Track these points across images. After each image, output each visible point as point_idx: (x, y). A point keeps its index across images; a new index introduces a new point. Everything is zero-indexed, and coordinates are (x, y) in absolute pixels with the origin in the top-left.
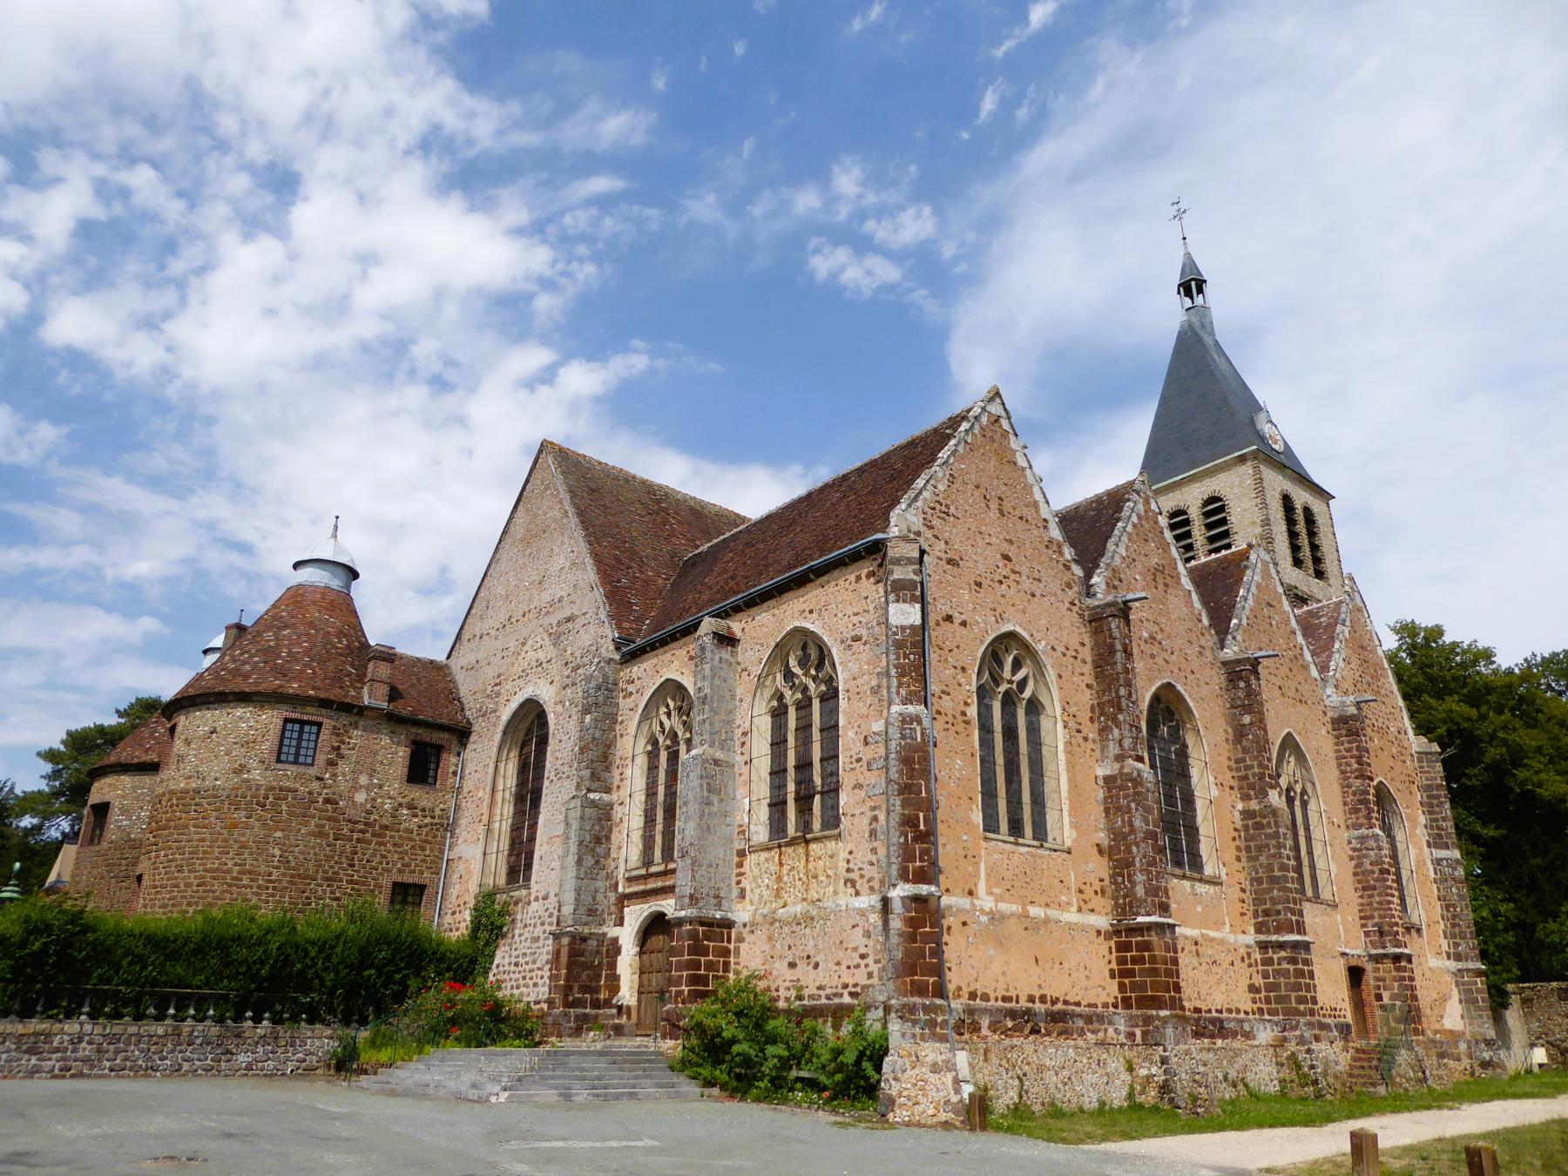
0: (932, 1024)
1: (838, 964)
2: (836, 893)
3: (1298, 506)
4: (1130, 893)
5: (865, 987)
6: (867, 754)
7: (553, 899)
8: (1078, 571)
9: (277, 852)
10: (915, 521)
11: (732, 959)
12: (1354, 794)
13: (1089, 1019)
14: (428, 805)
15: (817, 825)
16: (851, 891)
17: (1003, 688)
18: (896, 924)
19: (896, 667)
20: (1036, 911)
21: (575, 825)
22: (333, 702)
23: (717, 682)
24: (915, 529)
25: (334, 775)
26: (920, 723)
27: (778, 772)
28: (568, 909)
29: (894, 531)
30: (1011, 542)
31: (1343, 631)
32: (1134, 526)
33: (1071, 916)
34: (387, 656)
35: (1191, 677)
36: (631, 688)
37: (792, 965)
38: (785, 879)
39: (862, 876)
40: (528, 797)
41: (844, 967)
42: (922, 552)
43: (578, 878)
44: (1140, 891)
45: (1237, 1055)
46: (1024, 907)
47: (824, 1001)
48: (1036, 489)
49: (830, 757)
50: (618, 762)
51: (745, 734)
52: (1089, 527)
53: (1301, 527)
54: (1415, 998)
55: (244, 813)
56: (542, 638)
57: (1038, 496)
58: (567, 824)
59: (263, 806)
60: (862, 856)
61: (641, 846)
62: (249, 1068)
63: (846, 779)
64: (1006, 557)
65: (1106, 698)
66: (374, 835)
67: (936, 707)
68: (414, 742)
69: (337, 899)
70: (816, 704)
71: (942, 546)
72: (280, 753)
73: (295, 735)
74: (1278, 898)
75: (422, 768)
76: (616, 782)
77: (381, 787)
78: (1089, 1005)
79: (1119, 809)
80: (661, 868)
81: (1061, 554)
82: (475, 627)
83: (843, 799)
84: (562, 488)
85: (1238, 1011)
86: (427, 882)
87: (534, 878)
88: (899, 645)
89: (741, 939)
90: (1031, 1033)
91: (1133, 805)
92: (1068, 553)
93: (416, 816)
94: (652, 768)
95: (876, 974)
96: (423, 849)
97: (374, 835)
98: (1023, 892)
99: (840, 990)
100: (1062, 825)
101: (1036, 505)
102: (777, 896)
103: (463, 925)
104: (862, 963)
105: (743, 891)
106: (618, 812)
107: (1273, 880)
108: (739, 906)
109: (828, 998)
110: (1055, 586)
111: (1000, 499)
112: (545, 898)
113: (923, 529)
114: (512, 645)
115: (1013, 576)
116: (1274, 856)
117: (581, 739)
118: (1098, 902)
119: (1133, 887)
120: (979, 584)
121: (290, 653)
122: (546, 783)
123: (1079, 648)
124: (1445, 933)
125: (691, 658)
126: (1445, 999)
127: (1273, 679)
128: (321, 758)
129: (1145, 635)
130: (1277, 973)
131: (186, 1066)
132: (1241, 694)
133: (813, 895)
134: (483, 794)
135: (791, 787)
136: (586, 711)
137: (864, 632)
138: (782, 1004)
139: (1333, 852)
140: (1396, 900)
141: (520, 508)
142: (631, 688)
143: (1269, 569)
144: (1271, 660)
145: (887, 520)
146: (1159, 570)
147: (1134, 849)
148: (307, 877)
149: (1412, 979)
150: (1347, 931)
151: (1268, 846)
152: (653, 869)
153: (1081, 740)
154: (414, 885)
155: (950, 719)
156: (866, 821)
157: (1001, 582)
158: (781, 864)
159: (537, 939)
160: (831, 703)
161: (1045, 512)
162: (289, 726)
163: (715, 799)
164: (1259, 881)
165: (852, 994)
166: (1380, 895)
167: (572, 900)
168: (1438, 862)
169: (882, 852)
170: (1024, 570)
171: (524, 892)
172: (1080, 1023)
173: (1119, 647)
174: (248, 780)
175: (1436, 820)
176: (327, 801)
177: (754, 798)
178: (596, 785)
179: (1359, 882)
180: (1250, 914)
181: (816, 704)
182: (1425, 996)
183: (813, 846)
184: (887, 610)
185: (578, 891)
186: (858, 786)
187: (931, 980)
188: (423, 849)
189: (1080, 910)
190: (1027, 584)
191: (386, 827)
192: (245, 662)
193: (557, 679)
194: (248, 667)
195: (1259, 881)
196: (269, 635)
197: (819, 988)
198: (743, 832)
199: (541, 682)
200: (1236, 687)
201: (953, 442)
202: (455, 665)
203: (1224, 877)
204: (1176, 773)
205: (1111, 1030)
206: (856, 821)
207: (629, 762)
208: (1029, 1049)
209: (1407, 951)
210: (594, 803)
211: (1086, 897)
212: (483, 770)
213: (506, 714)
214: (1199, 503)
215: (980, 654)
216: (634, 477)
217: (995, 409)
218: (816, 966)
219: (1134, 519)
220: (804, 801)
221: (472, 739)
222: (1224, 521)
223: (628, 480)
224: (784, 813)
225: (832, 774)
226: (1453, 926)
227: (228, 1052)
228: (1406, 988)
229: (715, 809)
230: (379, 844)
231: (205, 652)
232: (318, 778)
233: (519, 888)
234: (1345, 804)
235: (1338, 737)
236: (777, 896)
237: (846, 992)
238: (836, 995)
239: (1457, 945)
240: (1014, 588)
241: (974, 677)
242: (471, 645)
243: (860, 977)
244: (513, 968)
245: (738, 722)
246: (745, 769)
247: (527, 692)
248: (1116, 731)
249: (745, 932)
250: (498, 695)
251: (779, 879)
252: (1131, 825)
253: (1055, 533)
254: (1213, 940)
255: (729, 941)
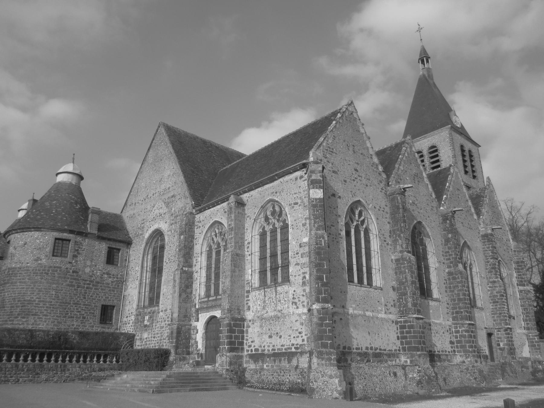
0: (330, 359)
1: (290, 336)
2: (288, 307)
3: (467, 149)
4: (406, 305)
5: (301, 345)
6: (302, 251)
7: (169, 311)
8: (384, 176)
9: (54, 293)
10: (320, 154)
11: (245, 335)
12: (490, 265)
13: (389, 356)
14: (115, 273)
15: (280, 280)
16: (295, 306)
17: (355, 223)
18: (315, 320)
19: (313, 215)
20: (368, 314)
21: (178, 281)
22: (75, 231)
23: (237, 222)
24: (319, 158)
25: (76, 261)
26: (323, 238)
27: (263, 258)
28: (176, 315)
29: (311, 159)
30: (358, 164)
31: (487, 200)
32: (406, 157)
33: (382, 315)
34: (98, 212)
35: (428, 219)
36: (200, 225)
37: (270, 337)
38: (267, 302)
39: (299, 301)
40: (157, 270)
41: (292, 337)
42: (323, 168)
43: (179, 302)
44: (410, 305)
45: (445, 368)
46: (364, 313)
47: (284, 351)
48: (367, 142)
49: (285, 251)
50: (195, 255)
51: (249, 243)
52: (388, 158)
53: (467, 158)
54: (513, 345)
55: (39, 277)
56: (161, 204)
57: (369, 145)
58: (175, 281)
59: (48, 274)
60: (300, 291)
61: (205, 289)
62: (47, 380)
63: (292, 261)
64: (356, 170)
65: (396, 228)
66: (93, 285)
67: (329, 231)
68: (109, 248)
69: (79, 312)
70: (279, 230)
71: (330, 165)
72: (54, 252)
73: (60, 245)
74: (464, 306)
75: (111, 258)
76: (194, 263)
77: (96, 266)
78: (389, 350)
79: (401, 272)
80: (214, 298)
81: (378, 169)
82: (132, 200)
83: (291, 269)
84: (168, 142)
85: (446, 351)
86: (116, 304)
87: (161, 302)
88: (314, 206)
89: (248, 327)
90: (367, 362)
91: (407, 271)
92: (380, 168)
93: (110, 277)
94: (209, 257)
95: (306, 340)
96: (114, 291)
97: (93, 285)
98: (364, 306)
99: (290, 346)
100: (377, 280)
101: (368, 148)
102: (264, 308)
103: (131, 322)
104: (300, 335)
105: (249, 307)
106: (195, 275)
107: (460, 300)
108: (248, 313)
109: (285, 349)
110: (376, 182)
111: (353, 146)
112: (166, 310)
113: (323, 158)
114: (149, 207)
115: (359, 178)
116: (460, 290)
117: (179, 246)
118: (393, 309)
119: (407, 303)
120: (345, 181)
121: (56, 211)
122: (165, 264)
123: (385, 207)
124: (523, 319)
125: (225, 212)
126: (523, 345)
127: (460, 220)
128: (70, 254)
129: (411, 202)
130: (461, 336)
131: (21, 379)
132: (448, 226)
133: (279, 308)
134: (138, 268)
135: (268, 265)
136: (181, 234)
137: (299, 201)
138: (266, 352)
139: (482, 288)
140: (506, 307)
141: (151, 150)
142: (200, 225)
143: (457, 176)
144: (459, 212)
145: (308, 154)
146: (416, 175)
147: (407, 288)
148: (66, 303)
149: (512, 338)
150: (487, 319)
151: (458, 286)
152: (211, 299)
153: (386, 245)
154: (110, 306)
155: (335, 237)
156: (301, 277)
157: (354, 180)
158: (265, 296)
159: (163, 327)
160: (285, 230)
161: (371, 152)
162: (57, 241)
163: (237, 270)
164: (454, 300)
165: (295, 348)
166: (500, 305)
167: (177, 312)
168: (521, 291)
169: (308, 290)
170: (364, 176)
171: (157, 308)
172: (385, 357)
173: (401, 207)
174: (39, 264)
175: (520, 275)
176: (73, 272)
177: (253, 269)
178: (186, 264)
179: (492, 300)
180: (450, 313)
181: (279, 230)
182: (517, 343)
183: (279, 288)
184: (309, 192)
185: (180, 308)
186: (297, 264)
187: (329, 342)
188: (114, 291)
189: (385, 313)
190: (364, 181)
191: (98, 283)
192: (38, 215)
193: (168, 221)
194: (39, 217)
195: (454, 300)
196: (47, 204)
197: (282, 346)
198: (249, 283)
199: (161, 222)
200: (446, 222)
201: (334, 122)
202: (125, 216)
203: (441, 298)
204: (421, 257)
205: (398, 360)
206: (296, 278)
207: (199, 255)
208: (367, 368)
209: (510, 327)
210: (185, 272)
211: (388, 308)
212: (136, 259)
213: (147, 235)
214: (427, 148)
215: (346, 210)
216: (197, 138)
217: (350, 109)
218: (280, 337)
219: (406, 155)
220: (274, 270)
221: (132, 246)
222: (437, 156)
223: (196, 138)
224: (266, 275)
225: (286, 259)
226: (527, 316)
227: (37, 374)
228: (510, 341)
229: (237, 274)
230: (95, 289)
231: (19, 211)
232: (70, 263)
233: (154, 306)
234: (486, 269)
235: (484, 242)
236: (264, 308)
237: (293, 348)
238: (289, 348)
239: (528, 324)
240: (359, 182)
241: (344, 219)
242: (131, 207)
243: (299, 341)
244: (153, 339)
245: (246, 238)
246: (249, 258)
247: (156, 226)
248: (400, 241)
249: (250, 324)
250: (143, 227)
251: (264, 302)
252: (406, 278)
253: (376, 160)
254: (436, 323)
255: (244, 328)
